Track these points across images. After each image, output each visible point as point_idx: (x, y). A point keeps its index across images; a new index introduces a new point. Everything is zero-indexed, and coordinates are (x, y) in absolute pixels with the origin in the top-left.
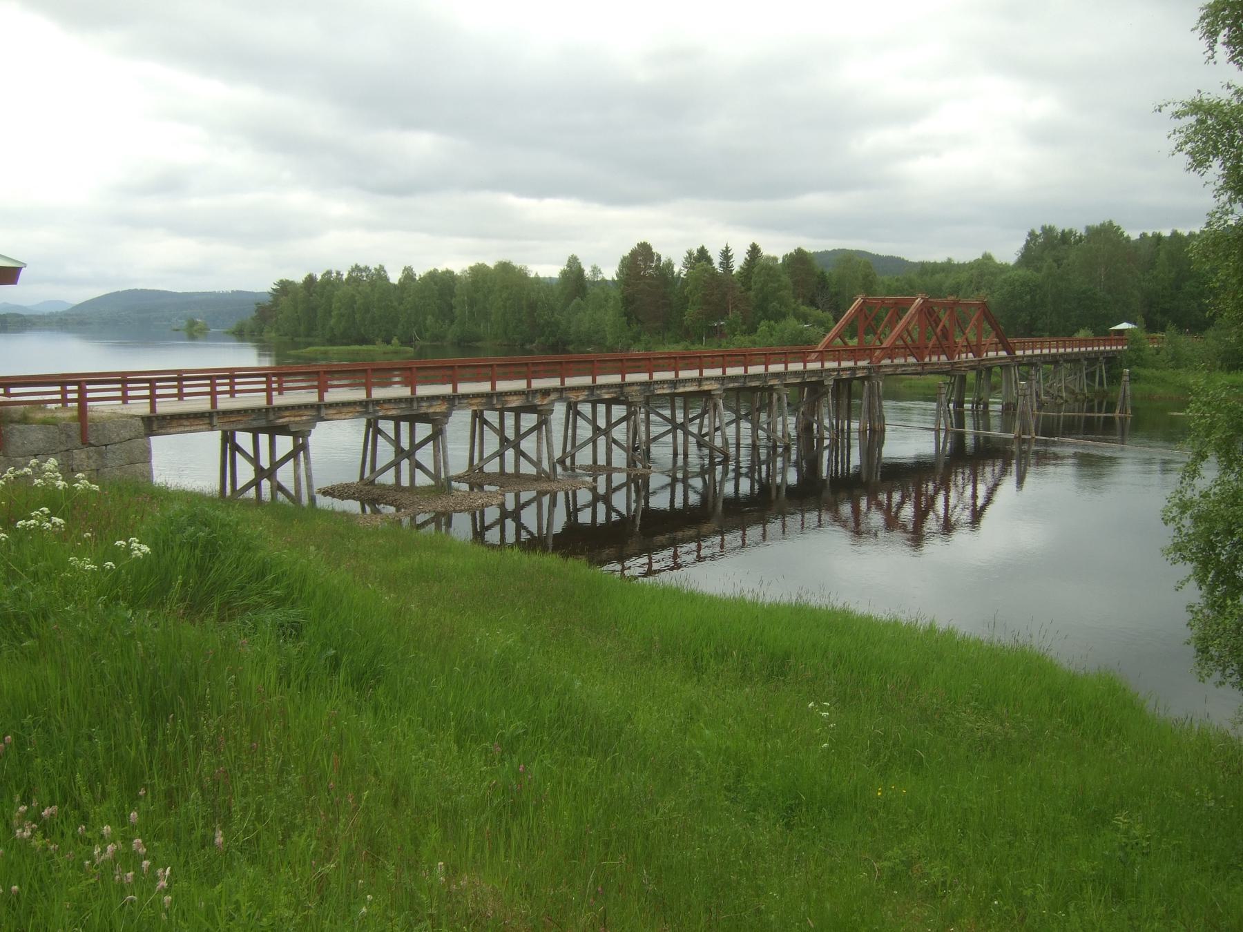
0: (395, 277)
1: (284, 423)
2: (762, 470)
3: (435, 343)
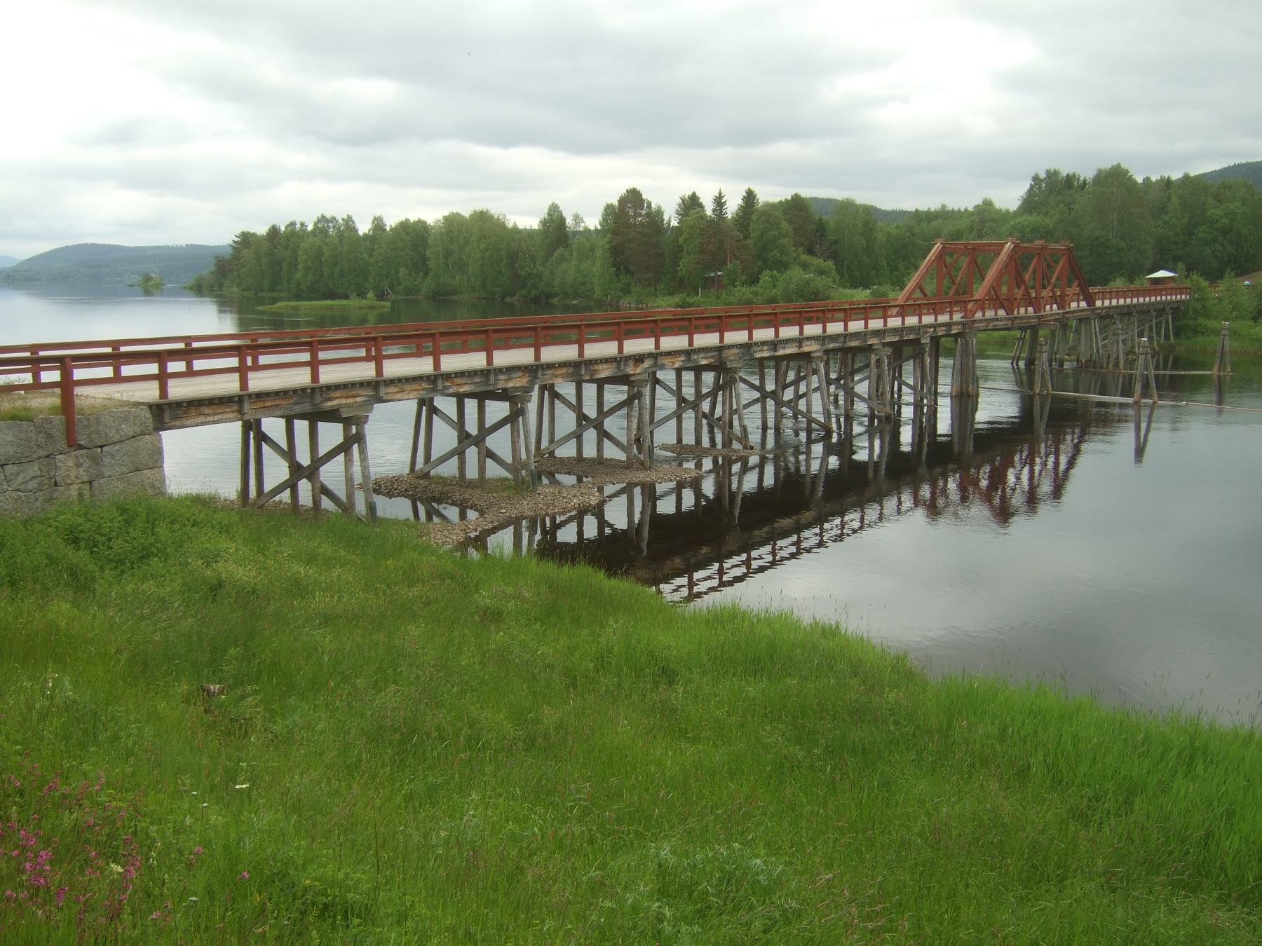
0: (364, 228)
1: (333, 406)
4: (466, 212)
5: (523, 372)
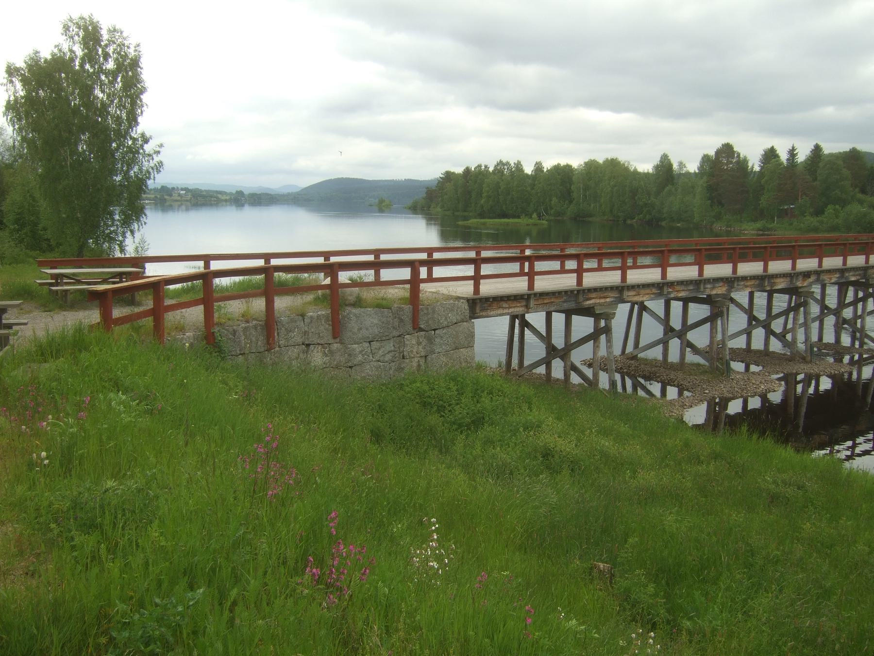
0: (529, 169)
2: (792, 319)
3: (558, 218)
4: (600, 159)
5: (724, 282)
